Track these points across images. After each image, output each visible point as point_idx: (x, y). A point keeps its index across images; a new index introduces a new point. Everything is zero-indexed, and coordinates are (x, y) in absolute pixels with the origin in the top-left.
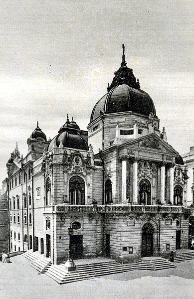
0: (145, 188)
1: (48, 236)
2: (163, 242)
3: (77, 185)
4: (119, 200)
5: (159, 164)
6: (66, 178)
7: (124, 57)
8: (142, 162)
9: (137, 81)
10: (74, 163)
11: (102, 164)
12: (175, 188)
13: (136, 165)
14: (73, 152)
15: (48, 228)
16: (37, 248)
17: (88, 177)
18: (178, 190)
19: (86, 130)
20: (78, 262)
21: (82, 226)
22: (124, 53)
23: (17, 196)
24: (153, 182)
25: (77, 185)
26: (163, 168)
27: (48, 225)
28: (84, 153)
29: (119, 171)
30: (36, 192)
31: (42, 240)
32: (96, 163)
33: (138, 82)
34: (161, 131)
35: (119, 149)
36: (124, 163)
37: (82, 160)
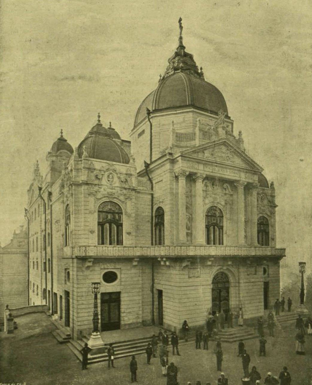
7: (181, 38)
9: (199, 71)
16: (57, 311)
17: (129, 203)
18: (214, 216)
22: (181, 33)
28: (121, 168)
31: (61, 297)
33: (202, 72)
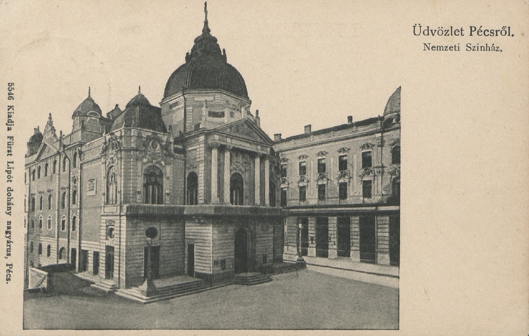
0: (237, 182)
1: (110, 249)
2: (259, 253)
3: (153, 178)
4: (207, 200)
5: (253, 155)
6: (141, 168)
8: (236, 151)
9: (222, 53)
10: (150, 149)
11: (183, 152)
12: (231, 178)
13: (227, 155)
14: (150, 134)
15: (109, 238)
19: (159, 106)
20: (158, 284)
21: (159, 234)
23: (49, 191)
24: (246, 177)
25: (153, 178)
26: (258, 160)
27: (110, 233)
29: (208, 162)
30: (87, 185)
31: (96, 255)
32: (176, 150)
34: (255, 115)
35: (208, 134)
36: (215, 152)
37: (161, 145)
